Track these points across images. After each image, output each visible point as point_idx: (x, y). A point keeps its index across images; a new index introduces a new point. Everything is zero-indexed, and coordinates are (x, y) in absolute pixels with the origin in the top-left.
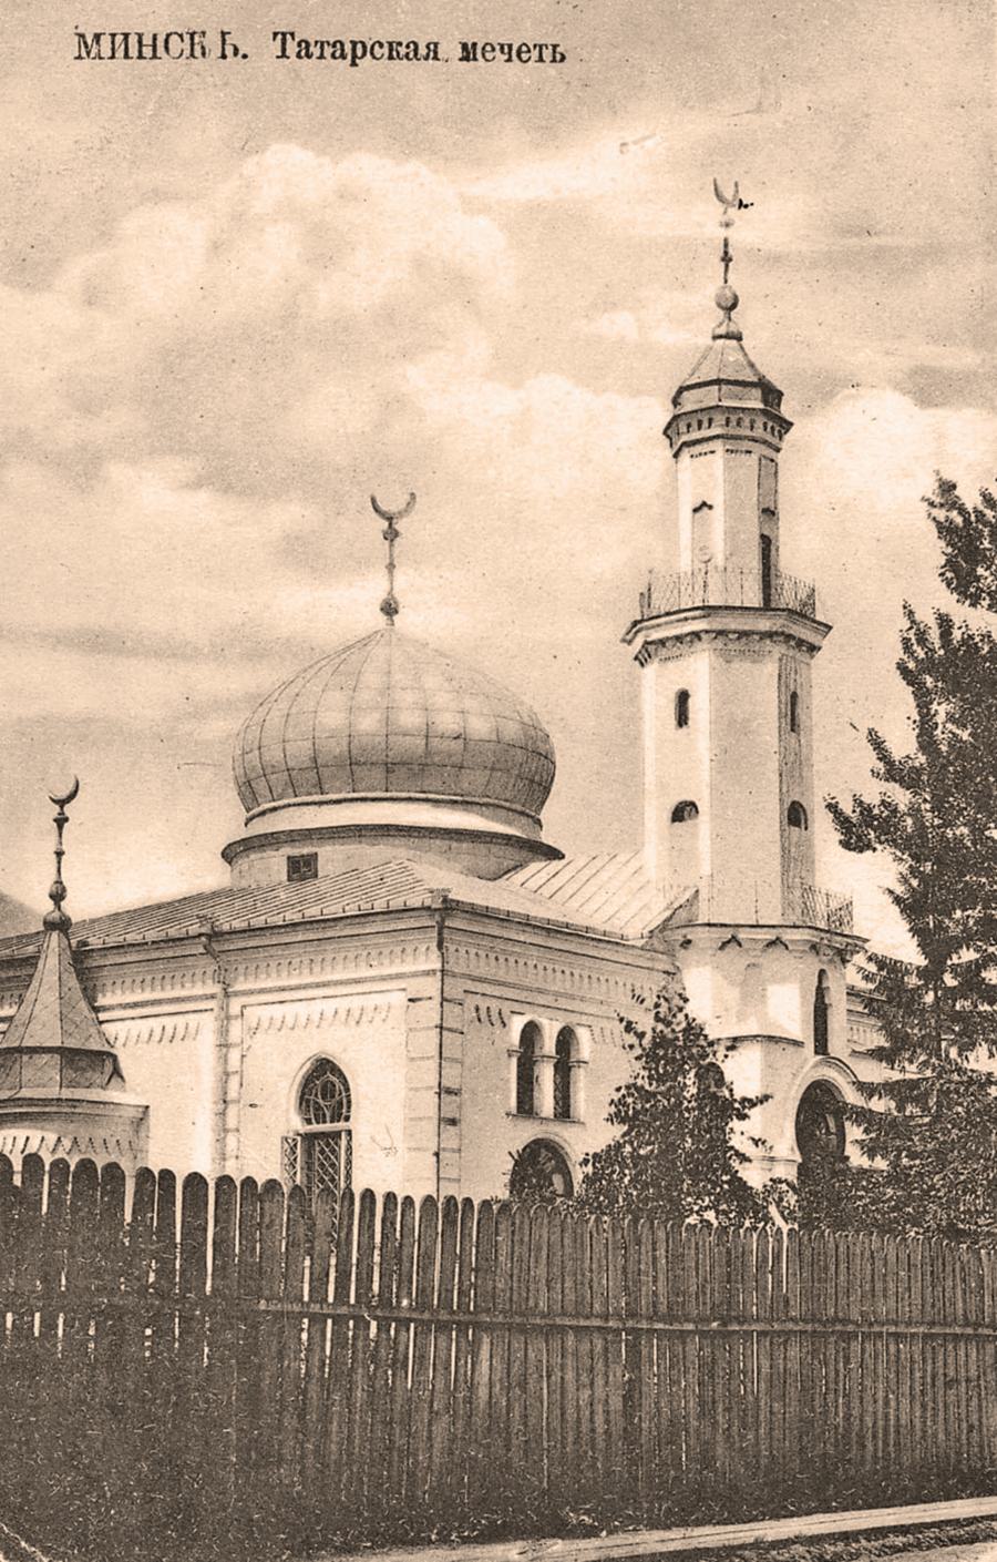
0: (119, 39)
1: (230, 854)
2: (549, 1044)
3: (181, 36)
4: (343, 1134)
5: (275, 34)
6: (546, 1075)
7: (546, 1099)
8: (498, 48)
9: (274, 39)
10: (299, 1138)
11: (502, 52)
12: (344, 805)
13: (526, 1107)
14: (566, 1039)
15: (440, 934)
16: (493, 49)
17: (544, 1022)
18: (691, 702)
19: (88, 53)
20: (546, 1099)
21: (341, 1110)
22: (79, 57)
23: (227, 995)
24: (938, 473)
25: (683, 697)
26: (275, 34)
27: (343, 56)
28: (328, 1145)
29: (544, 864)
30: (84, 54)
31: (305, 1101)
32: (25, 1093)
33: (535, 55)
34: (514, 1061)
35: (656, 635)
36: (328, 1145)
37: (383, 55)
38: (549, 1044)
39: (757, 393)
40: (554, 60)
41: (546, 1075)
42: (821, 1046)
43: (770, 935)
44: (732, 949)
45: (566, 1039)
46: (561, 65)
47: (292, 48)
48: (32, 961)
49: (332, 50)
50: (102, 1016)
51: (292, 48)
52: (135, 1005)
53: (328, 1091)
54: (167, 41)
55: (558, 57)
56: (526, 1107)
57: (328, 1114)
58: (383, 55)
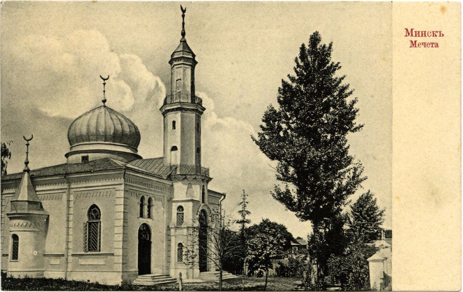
0: (417, 33)
1: (67, 156)
4: (99, 223)
6: (146, 208)
7: (146, 213)
10: (88, 223)
12: (103, 145)
13: (142, 215)
14: (150, 200)
15: (124, 175)
17: (145, 197)
18: (176, 124)
20: (146, 213)
21: (98, 217)
23: (70, 189)
24: (354, 90)
28: (95, 225)
29: (139, 160)
31: (89, 215)
32: (19, 212)
34: (139, 205)
35: (167, 109)
36: (95, 225)
37: (431, 35)
39: (191, 54)
40: (440, 36)
41: (146, 208)
42: (203, 202)
43: (194, 177)
44: (186, 180)
46: (442, 37)
48: (20, 179)
50: (38, 193)
52: (61, 189)
53: (95, 211)
54: (428, 33)
55: (441, 35)
56: (142, 215)
57: (95, 217)
58: (431, 35)
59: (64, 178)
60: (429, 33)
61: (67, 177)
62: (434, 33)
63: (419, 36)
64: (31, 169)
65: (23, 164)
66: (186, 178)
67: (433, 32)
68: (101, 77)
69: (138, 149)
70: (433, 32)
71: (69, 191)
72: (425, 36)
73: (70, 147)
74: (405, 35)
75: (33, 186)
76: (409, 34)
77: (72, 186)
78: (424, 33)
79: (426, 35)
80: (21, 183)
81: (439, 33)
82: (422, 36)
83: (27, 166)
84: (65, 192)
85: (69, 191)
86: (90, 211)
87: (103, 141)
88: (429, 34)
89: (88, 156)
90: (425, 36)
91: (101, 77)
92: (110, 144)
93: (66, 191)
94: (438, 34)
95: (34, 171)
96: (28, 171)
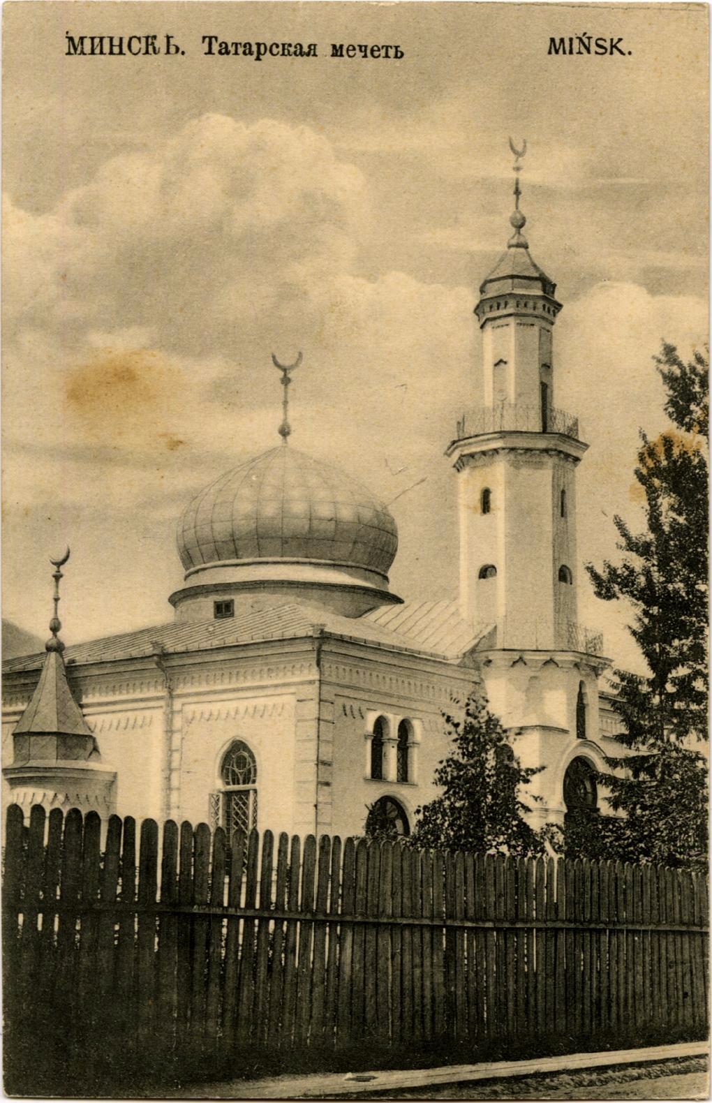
2: (393, 731)
3: (139, 39)
4: (251, 792)
5: (204, 38)
6: (392, 754)
8: (357, 48)
9: (203, 42)
11: (361, 51)
13: (377, 773)
14: (405, 727)
16: (354, 49)
19: (75, 49)
21: (249, 776)
22: (69, 53)
23: (171, 697)
25: (486, 494)
26: (204, 38)
27: (251, 53)
28: (241, 799)
30: (72, 51)
33: (383, 52)
38: (393, 731)
40: (396, 57)
41: (392, 754)
42: (581, 733)
45: (405, 727)
47: (215, 48)
48: (38, 672)
49: (243, 49)
51: (215, 48)
53: (241, 762)
55: (399, 54)
56: (377, 773)
59: (154, 666)
60: (135, 41)
61: (165, 664)
62: (286, 46)
63: (101, 53)
64: (67, 644)
65: (523, 753)
66: (521, 659)
67: (284, 45)
68: (274, 357)
69: (390, 574)
70: (284, 45)
71: (170, 705)
72: (121, 53)
73: (184, 573)
74: (67, 51)
75: (73, 692)
76: (75, 49)
77: (178, 692)
78: (116, 42)
79: (125, 49)
80: (39, 686)
81: (394, 50)
82: (93, 53)
83: (55, 635)
84: (161, 707)
85: (170, 705)
86: (227, 758)
87: (277, 556)
88: (275, 50)
89: (232, 601)
90: (121, 53)
91: (274, 357)
92: (298, 563)
93: (162, 703)
94: (392, 52)
95: (78, 647)
96: (58, 648)
